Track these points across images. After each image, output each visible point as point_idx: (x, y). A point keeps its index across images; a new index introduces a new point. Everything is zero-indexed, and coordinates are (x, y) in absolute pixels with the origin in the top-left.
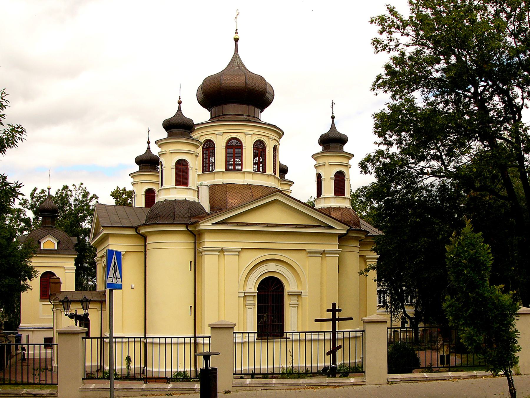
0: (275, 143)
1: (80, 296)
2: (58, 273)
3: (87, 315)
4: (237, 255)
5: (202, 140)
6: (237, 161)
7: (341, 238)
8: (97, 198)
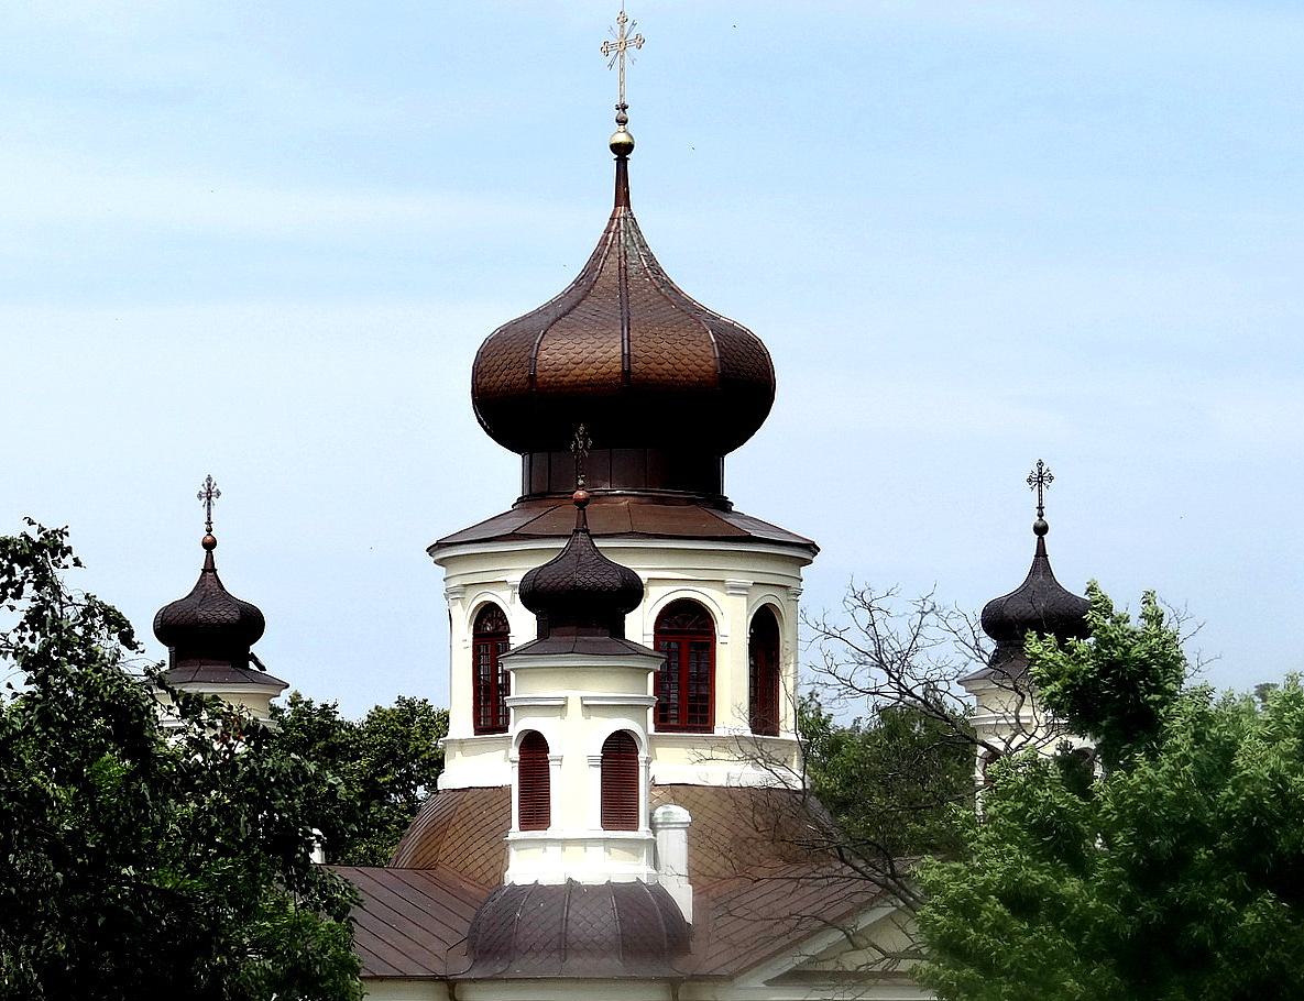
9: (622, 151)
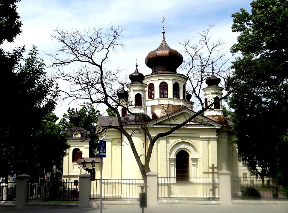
0: (184, 83)
1: (91, 160)
2: (81, 149)
3: (94, 169)
4: (165, 140)
5: (148, 84)
6: (165, 93)
7: (218, 131)
8: (99, 112)
9: (164, 33)
